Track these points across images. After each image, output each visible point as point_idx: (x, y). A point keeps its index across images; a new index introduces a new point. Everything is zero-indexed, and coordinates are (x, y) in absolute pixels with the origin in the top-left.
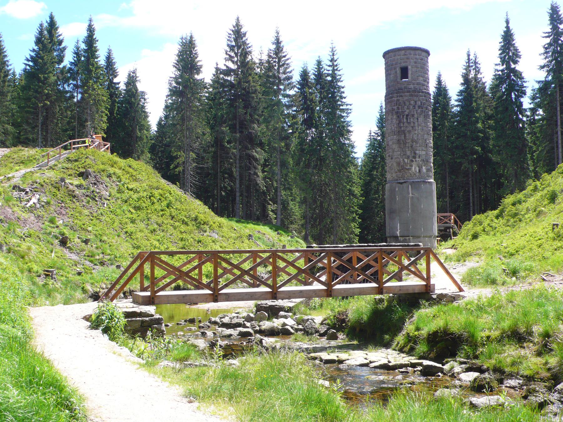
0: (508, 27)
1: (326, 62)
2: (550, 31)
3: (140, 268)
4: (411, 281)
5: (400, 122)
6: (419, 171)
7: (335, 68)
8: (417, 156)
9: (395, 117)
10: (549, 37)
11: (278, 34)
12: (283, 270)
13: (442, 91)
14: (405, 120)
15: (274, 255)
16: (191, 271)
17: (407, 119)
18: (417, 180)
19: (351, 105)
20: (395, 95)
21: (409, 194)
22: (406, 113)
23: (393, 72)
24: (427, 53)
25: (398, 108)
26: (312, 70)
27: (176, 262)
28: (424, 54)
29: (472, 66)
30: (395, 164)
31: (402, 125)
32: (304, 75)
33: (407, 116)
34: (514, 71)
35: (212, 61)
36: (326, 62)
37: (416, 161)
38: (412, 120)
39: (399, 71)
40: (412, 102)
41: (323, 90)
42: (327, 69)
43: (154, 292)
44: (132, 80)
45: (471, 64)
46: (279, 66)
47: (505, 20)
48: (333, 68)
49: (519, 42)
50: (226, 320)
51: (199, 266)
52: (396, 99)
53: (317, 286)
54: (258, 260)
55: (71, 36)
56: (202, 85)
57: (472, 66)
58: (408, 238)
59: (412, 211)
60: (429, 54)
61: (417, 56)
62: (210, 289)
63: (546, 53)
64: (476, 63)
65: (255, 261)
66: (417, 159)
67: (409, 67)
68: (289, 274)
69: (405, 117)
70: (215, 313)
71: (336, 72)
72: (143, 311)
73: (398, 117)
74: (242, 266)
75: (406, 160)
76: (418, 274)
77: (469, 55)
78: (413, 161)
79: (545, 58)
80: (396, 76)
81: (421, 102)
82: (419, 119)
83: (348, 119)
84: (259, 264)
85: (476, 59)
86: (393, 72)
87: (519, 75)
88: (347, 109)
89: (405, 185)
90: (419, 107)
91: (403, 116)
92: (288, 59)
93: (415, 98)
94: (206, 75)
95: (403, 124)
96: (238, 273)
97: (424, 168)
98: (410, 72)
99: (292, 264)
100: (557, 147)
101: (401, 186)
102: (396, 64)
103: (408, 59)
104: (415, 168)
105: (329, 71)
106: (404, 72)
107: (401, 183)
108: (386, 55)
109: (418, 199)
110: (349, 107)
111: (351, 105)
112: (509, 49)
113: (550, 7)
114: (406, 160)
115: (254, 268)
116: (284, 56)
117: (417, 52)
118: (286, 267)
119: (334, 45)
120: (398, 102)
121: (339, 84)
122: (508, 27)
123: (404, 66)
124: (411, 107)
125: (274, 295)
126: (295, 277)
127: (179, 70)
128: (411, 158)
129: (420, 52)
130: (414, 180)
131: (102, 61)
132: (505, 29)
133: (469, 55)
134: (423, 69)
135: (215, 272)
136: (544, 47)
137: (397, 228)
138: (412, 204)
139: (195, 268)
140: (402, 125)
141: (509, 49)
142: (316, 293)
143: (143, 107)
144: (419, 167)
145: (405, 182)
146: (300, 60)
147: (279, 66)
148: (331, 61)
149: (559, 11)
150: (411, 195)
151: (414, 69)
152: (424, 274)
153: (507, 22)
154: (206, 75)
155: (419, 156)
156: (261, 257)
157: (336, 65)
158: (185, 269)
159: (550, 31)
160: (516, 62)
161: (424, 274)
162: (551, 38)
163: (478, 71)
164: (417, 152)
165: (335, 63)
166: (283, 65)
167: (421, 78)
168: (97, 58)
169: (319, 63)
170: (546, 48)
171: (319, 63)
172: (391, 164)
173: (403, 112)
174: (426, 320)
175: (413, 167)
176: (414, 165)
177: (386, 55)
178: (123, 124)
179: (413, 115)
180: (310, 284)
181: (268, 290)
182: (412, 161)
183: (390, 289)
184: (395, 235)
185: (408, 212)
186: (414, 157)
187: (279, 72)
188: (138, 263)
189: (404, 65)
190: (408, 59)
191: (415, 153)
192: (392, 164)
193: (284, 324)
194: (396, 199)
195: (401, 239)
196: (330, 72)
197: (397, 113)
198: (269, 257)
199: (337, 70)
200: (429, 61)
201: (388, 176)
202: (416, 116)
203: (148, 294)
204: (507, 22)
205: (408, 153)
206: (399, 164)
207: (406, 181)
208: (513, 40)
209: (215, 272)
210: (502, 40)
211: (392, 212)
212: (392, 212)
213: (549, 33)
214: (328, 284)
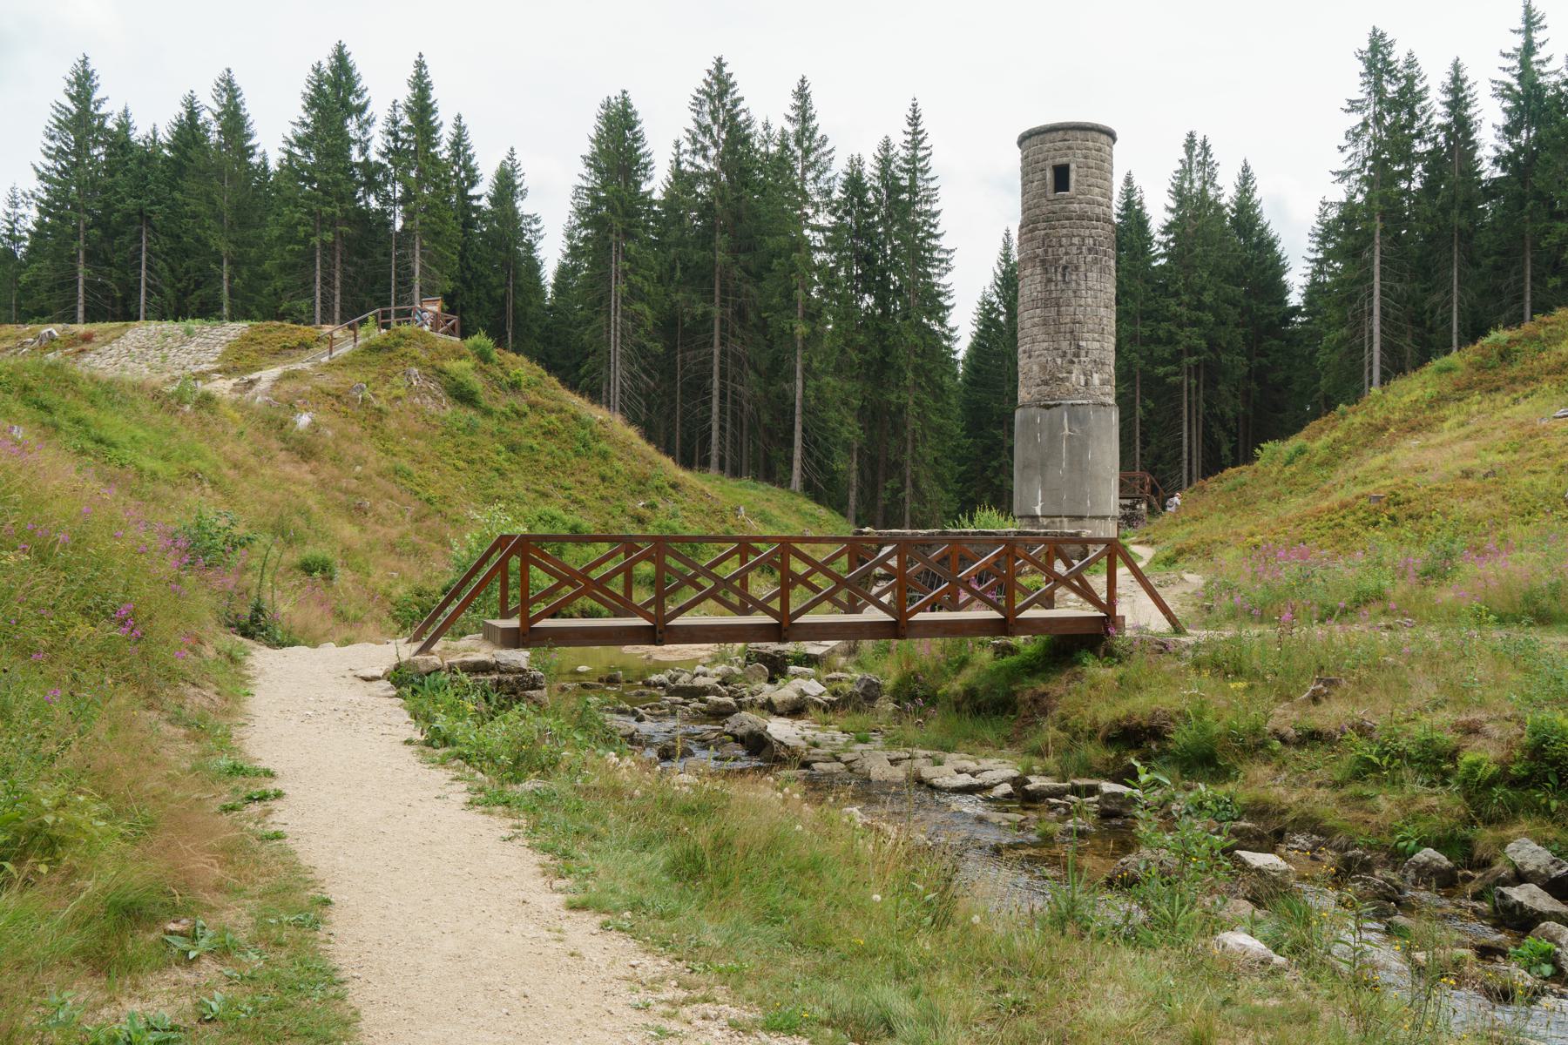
3: (503, 565)
4: (1070, 607)
6: (1086, 384)
9: (1039, 270)
12: (803, 580)
13: (1134, 218)
15: (786, 546)
16: (608, 577)
20: (1041, 225)
22: (1063, 262)
23: (1039, 176)
24: (1111, 135)
25: (1046, 252)
27: (574, 556)
28: (1104, 138)
30: (1035, 368)
32: (855, 184)
33: (1065, 268)
35: (667, 142)
36: (899, 140)
39: (1049, 175)
41: (890, 216)
43: (527, 621)
44: (507, 185)
46: (806, 169)
50: (684, 680)
51: (627, 570)
53: (872, 614)
54: (752, 559)
55: (383, 94)
56: (646, 199)
59: (1070, 464)
60: (1114, 140)
61: (1090, 144)
62: (647, 616)
65: (744, 560)
67: (1073, 166)
68: (815, 589)
70: (661, 667)
72: (502, 660)
73: (1046, 271)
74: (719, 570)
75: (1059, 361)
76: (1087, 593)
80: (1044, 185)
83: (942, 281)
84: (752, 567)
86: (1039, 176)
90: (1090, 250)
93: (1082, 232)
94: (656, 184)
96: (709, 584)
97: (1096, 376)
98: (1073, 176)
99: (816, 567)
103: (1069, 148)
104: (1077, 377)
106: (1062, 176)
107: (1048, 407)
108: (1024, 139)
114: (1059, 361)
115: (742, 576)
117: (1090, 135)
118: (809, 574)
123: (1060, 161)
124: (1074, 250)
125: (781, 631)
126: (829, 596)
127: (599, 170)
128: (1069, 356)
129: (1096, 135)
131: (443, 151)
134: (1103, 167)
135: (654, 579)
139: (616, 572)
142: (874, 630)
143: (530, 247)
146: (853, 139)
147: (806, 169)
150: (1067, 432)
152: (1103, 596)
154: (656, 184)
156: (757, 552)
158: (595, 574)
161: (1103, 596)
163: (1209, 180)
164: (1083, 344)
166: (813, 165)
167: (1097, 190)
168: (434, 145)
172: (1028, 367)
174: (1096, 696)
176: (1076, 369)
178: (473, 259)
179: (1077, 268)
180: (858, 610)
181: (769, 620)
182: (1072, 362)
183: (1032, 626)
185: (1060, 467)
186: (1077, 355)
187: (803, 179)
188: (496, 558)
190: (1069, 148)
191: (1079, 347)
192: (1030, 370)
193: (802, 693)
195: (1045, 521)
197: (1043, 262)
198: (785, 604)
200: (1114, 153)
201: (1023, 395)
202: (1082, 269)
203: (515, 623)
205: (1065, 345)
206: (1043, 367)
209: (654, 579)
214: (899, 609)
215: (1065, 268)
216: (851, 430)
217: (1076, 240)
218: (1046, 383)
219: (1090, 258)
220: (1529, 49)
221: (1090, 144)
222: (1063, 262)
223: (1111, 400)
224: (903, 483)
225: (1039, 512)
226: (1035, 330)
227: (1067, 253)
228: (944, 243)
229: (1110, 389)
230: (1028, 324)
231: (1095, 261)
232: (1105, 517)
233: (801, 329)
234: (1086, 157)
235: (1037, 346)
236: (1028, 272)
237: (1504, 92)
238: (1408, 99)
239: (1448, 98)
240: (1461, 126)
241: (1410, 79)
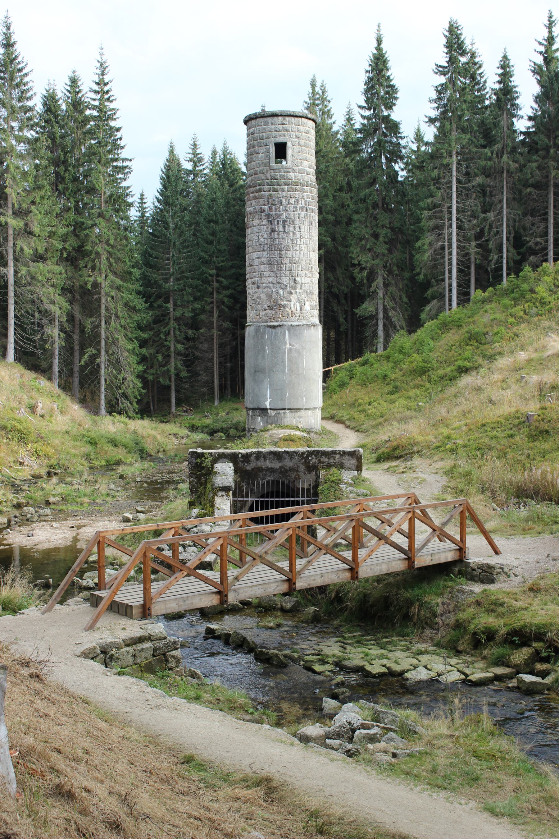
0: (379, 49)
1: (87, 86)
2: (446, 65)
5: (273, 231)
7: (106, 97)
8: (298, 286)
9: (265, 222)
10: (444, 74)
11: (8, 28)
14: (281, 229)
17: (284, 227)
18: (297, 323)
19: (130, 160)
21: (286, 344)
25: (270, 209)
26: (61, 91)
29: (318, 105)
30: (263, 297)
31: (276, 236)
32: (50, 102)
34: (387, 119)
37: (296, 293)
38: (292, 229)
40: (292, 201)
42: (88, 94)
45: (317, 102)
47: (375, 36)
48: (102, 96)
49: (396, 73)
52: (267, 193)
57: (318, 105)
58: (282, 412)
63: (440, 99)
64: (323, 99)
66: (298, 290)
67: (289, 145)
69: (281, 223)
71: (106, 103)
75: (281, 292)
77: (313, 85)
78: (292, 293)
79: (438, 108)
81: (306, 201)
82: (302, 227)
83: (124, 184)
85: (323, 93)
87: (394, 127)
88: (125, 167)
89: (279, 330)
91: (278, 221)
92: (26, 75)
95: (278, 234)
97: (307, 303)
98: (289, 152)
100: (450, 246)
101: (274, 331)
102: (268, 138)
103: (287, 130)
105: (95, 100)
107: (274, 327)
108: (247, 121)
109: (299, 352)
110: (126, 164)
111: (130, 160)
112: (379, 85)
113: (447, 26)
116: (20, 70)
119: (104, 58)
120: (270, 200)
121: (112, 123)
122: (379, 49)
128: (289, 289)
130: (293, 324)
132: (375, 52)
133: (313, 85)
136: (437, 91)
137: (266, 395)
138: (290, 360)
140: (276, 236)
141: (379, 85)
144: (300, 302)
145: (280, 326)
148: (98, 84)
149: (461, 34)
150: (288, 346)
151: (296, 148)
153: (379, 41)
155: (301, 286)
157: (108, 92)
159: (446, 65)
160: (389, 107)
161: (458, 537)
162: (447, 76)
164: (298, 279)
165: (106, 89)
169: (74, 81)
170: (439, 92)
171: (74, 81)
173: (279, 216)
175: (292, 303)
176: (293, 298)
177: (247, 121)
184: (262, 407)
189: (280, 140)
191: (295, 281)
194: (264, 351)
196: (97, 103)
197: (268, 216)
199: (108, 100)
202: (297, 223)
204: (379, 41)
206: (269, 296)
207: (281, 323)
208: (388, 70)
210: (369, 69)
211: (258, 370)
212: (258, 370)
213: (444, 67)
215: (285, 221)
216: (58, 306)
217: (292, 201)
218: (271, 308)
219: (302, 215)
220: (551, 40)
221: (301, 128)
222: (284, 217)
223: (316, 320)
224: (99, 351)
225: (268, 407)
226: (262, 267)
227: (286, 211)
228: (124, 154)
229: (316, 312)
230: (256, 262)
231: (306, 216)
232: (315, 409)
233: (14, 223)
234: (298, 137)
235: (264, 280)
236: (256, 222)
237: (537, 70)
238: (471, 71)
239: (500, 71)
240: (506, 93)
241: (473, 55)
